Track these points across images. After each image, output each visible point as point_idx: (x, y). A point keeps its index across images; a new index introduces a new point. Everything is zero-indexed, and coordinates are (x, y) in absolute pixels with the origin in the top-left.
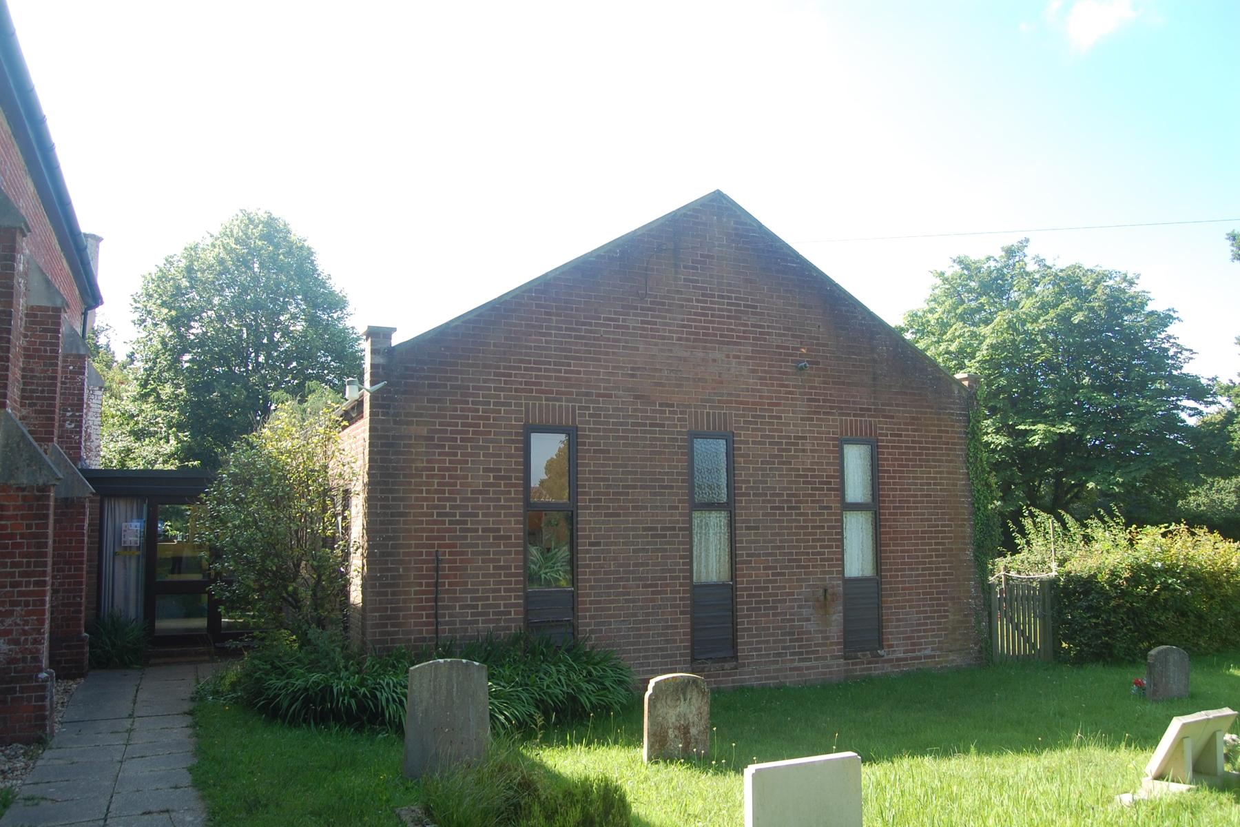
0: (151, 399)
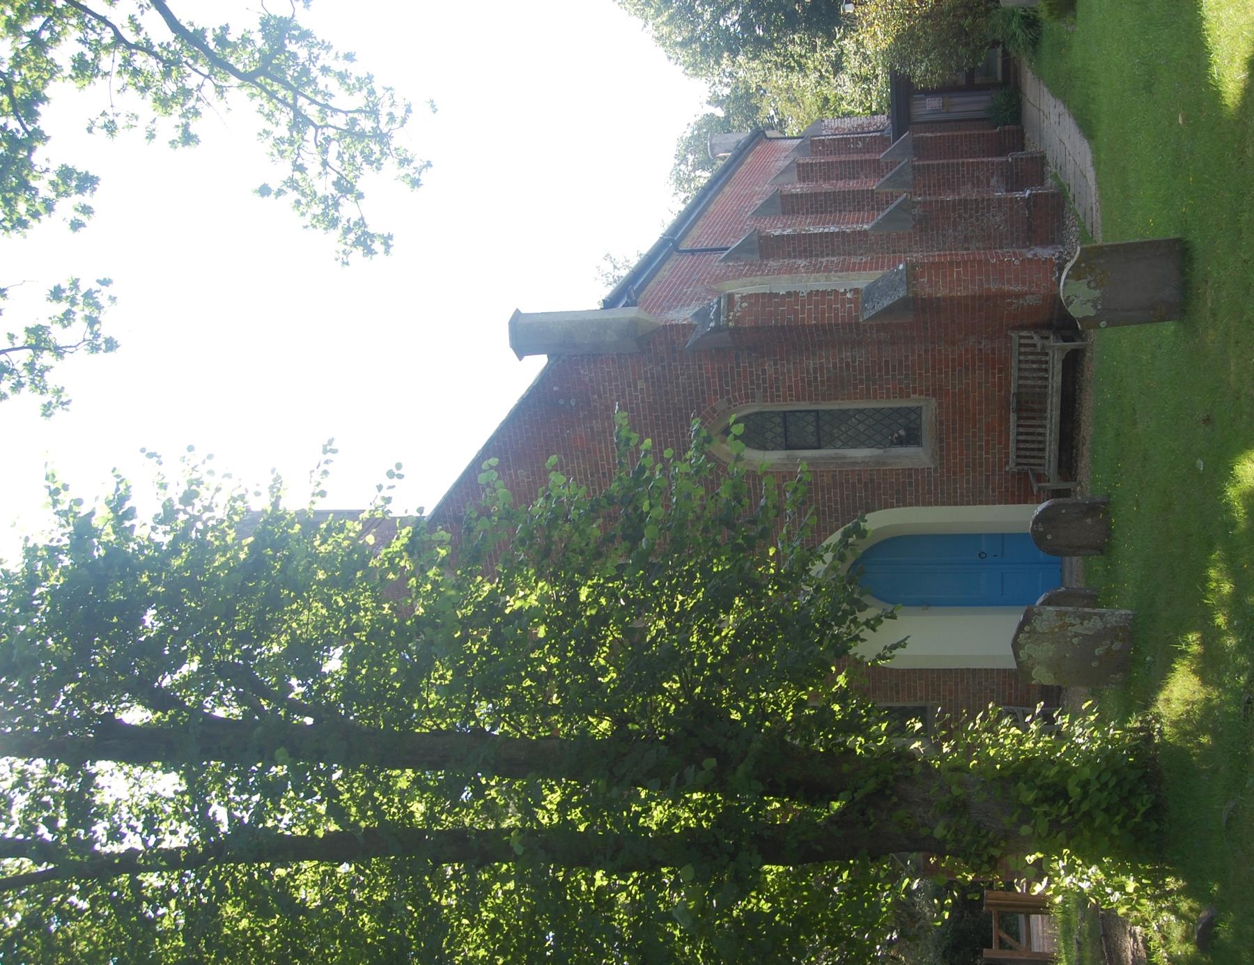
0: (803, 61)
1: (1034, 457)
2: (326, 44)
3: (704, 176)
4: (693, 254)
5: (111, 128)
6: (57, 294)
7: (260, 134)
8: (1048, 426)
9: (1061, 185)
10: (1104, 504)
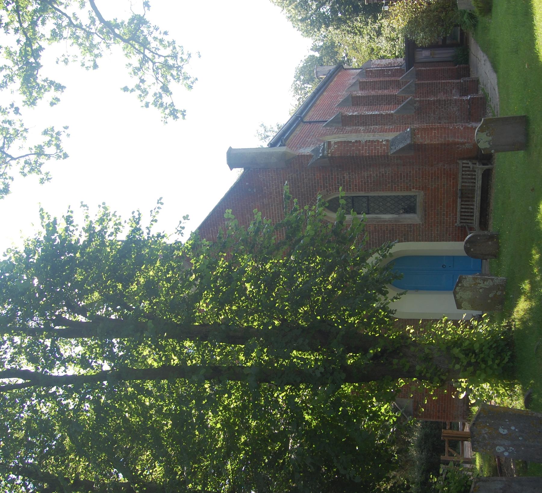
0: (362, 30)
1: (468, 219)
2: (157, 27)
3: (310, 88)
4: (310, 124)
5: (66, 62)
6: (45, 133)
7: (127, 65)
8: (475, 205)
9: (485, 93)
10: (497, 235)
